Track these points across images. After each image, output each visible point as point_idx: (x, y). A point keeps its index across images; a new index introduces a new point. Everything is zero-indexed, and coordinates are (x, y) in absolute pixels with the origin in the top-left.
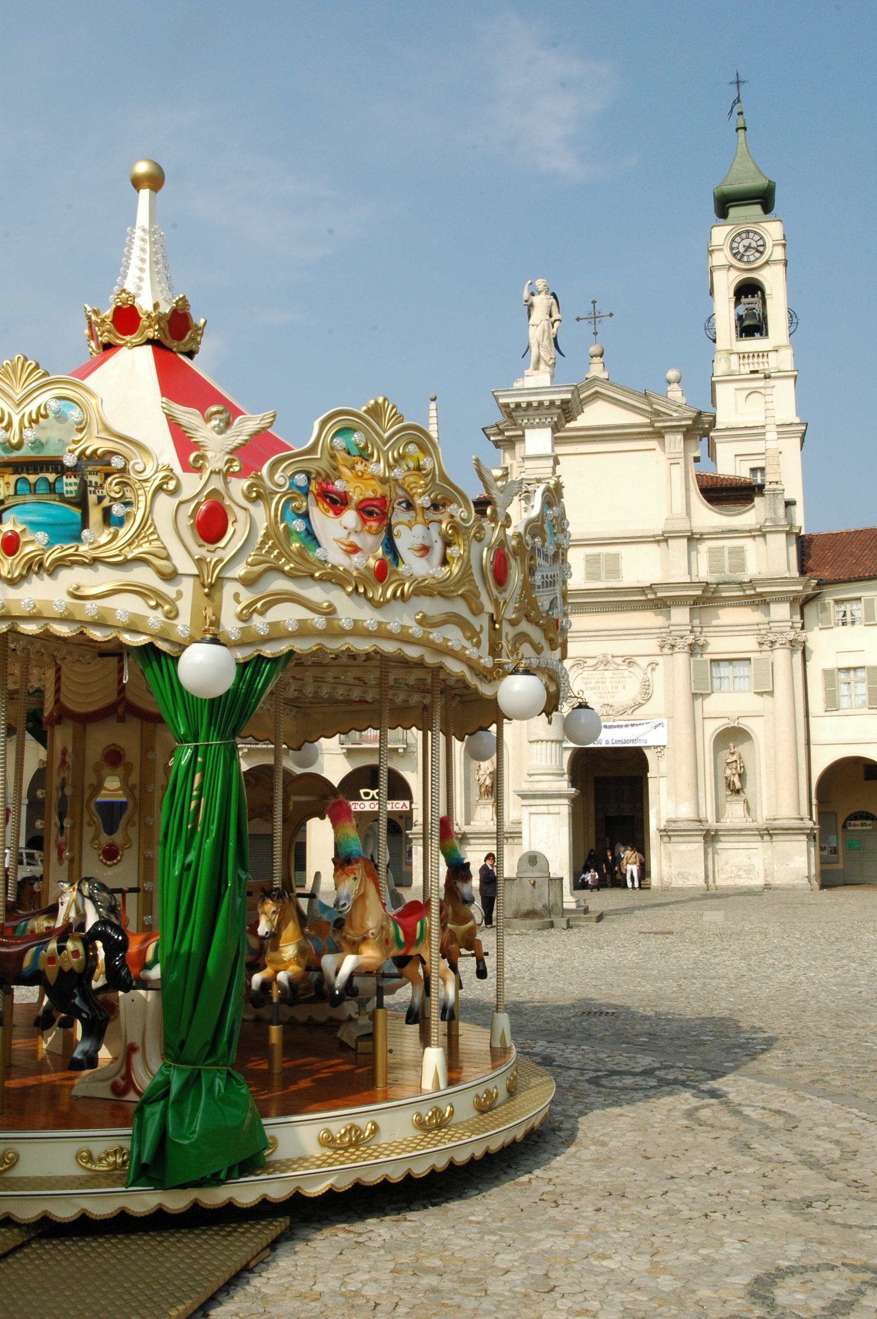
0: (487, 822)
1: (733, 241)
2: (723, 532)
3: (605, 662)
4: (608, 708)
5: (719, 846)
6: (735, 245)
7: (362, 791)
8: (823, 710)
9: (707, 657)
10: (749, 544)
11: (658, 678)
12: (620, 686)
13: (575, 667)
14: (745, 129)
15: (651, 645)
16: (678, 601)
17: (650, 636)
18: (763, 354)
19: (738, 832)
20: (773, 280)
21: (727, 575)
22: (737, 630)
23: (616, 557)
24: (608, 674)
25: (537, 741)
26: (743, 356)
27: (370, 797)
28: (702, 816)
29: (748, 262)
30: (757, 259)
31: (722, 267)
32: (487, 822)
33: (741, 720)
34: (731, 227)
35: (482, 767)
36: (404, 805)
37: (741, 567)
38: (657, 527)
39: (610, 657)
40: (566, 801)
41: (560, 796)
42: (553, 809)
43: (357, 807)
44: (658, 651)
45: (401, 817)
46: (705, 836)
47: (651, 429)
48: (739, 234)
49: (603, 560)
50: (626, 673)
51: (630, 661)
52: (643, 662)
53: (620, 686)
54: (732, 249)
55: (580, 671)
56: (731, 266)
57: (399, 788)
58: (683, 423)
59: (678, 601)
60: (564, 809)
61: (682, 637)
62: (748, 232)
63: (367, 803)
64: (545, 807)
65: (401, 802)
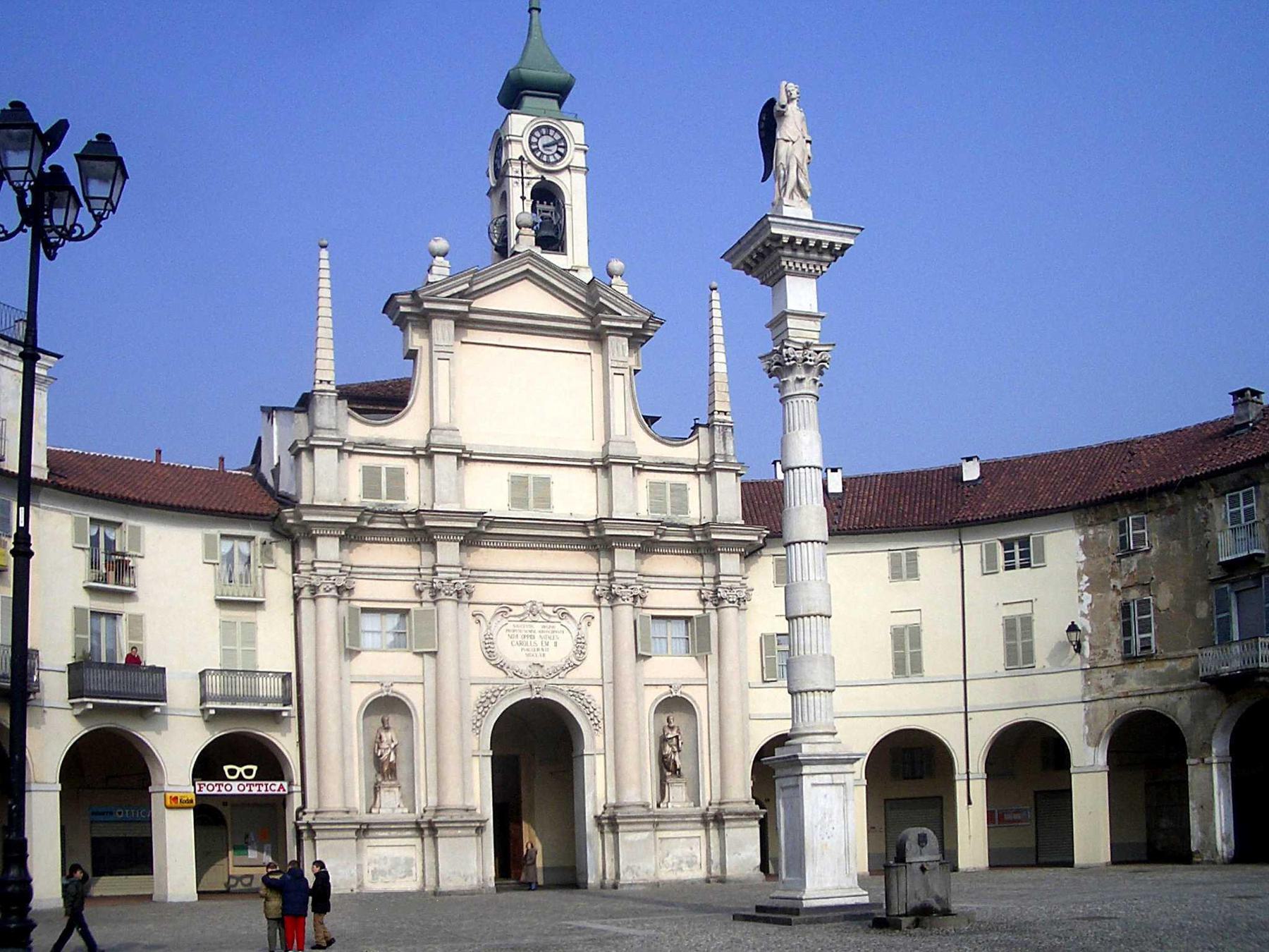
0: (393, 809)
1: (532, 134)
2: (664, 464)
3: (533, 611)
4: (536, 668)
5: (366, 842)
6: (534, 140)
7: (226, 768)
8: (1003, 669)
11: (592, 635)
12: (551, 643)
13: (499, 617)
14: (539, 10)
15: (583, 594)
17: (585, 583)
19: (680, 819)
20: (574, 188)
21: (667, 516)
22: (381, 573)
23: (546, 481)
24: (537, 626)
27: (237, 776)
28: (350, 806)
29: (548, 163)
30: (558, 161)
32: (393, 809)
33: (686, 690)
35: (384, 739)
36: (281, 786)
37: (683, 507)
39: (540, 605)
43: (263, 789)
45: (225, 804)
46: (358, 831)
47: (588, 328)
48: (539, 129)
51: (562, 611)
53: (551, 643)
54: (530, 143)
55: (505, 621)
57: (272, 765)
58: (633, 325)
60: (1104, 777)
62: (548, 128)
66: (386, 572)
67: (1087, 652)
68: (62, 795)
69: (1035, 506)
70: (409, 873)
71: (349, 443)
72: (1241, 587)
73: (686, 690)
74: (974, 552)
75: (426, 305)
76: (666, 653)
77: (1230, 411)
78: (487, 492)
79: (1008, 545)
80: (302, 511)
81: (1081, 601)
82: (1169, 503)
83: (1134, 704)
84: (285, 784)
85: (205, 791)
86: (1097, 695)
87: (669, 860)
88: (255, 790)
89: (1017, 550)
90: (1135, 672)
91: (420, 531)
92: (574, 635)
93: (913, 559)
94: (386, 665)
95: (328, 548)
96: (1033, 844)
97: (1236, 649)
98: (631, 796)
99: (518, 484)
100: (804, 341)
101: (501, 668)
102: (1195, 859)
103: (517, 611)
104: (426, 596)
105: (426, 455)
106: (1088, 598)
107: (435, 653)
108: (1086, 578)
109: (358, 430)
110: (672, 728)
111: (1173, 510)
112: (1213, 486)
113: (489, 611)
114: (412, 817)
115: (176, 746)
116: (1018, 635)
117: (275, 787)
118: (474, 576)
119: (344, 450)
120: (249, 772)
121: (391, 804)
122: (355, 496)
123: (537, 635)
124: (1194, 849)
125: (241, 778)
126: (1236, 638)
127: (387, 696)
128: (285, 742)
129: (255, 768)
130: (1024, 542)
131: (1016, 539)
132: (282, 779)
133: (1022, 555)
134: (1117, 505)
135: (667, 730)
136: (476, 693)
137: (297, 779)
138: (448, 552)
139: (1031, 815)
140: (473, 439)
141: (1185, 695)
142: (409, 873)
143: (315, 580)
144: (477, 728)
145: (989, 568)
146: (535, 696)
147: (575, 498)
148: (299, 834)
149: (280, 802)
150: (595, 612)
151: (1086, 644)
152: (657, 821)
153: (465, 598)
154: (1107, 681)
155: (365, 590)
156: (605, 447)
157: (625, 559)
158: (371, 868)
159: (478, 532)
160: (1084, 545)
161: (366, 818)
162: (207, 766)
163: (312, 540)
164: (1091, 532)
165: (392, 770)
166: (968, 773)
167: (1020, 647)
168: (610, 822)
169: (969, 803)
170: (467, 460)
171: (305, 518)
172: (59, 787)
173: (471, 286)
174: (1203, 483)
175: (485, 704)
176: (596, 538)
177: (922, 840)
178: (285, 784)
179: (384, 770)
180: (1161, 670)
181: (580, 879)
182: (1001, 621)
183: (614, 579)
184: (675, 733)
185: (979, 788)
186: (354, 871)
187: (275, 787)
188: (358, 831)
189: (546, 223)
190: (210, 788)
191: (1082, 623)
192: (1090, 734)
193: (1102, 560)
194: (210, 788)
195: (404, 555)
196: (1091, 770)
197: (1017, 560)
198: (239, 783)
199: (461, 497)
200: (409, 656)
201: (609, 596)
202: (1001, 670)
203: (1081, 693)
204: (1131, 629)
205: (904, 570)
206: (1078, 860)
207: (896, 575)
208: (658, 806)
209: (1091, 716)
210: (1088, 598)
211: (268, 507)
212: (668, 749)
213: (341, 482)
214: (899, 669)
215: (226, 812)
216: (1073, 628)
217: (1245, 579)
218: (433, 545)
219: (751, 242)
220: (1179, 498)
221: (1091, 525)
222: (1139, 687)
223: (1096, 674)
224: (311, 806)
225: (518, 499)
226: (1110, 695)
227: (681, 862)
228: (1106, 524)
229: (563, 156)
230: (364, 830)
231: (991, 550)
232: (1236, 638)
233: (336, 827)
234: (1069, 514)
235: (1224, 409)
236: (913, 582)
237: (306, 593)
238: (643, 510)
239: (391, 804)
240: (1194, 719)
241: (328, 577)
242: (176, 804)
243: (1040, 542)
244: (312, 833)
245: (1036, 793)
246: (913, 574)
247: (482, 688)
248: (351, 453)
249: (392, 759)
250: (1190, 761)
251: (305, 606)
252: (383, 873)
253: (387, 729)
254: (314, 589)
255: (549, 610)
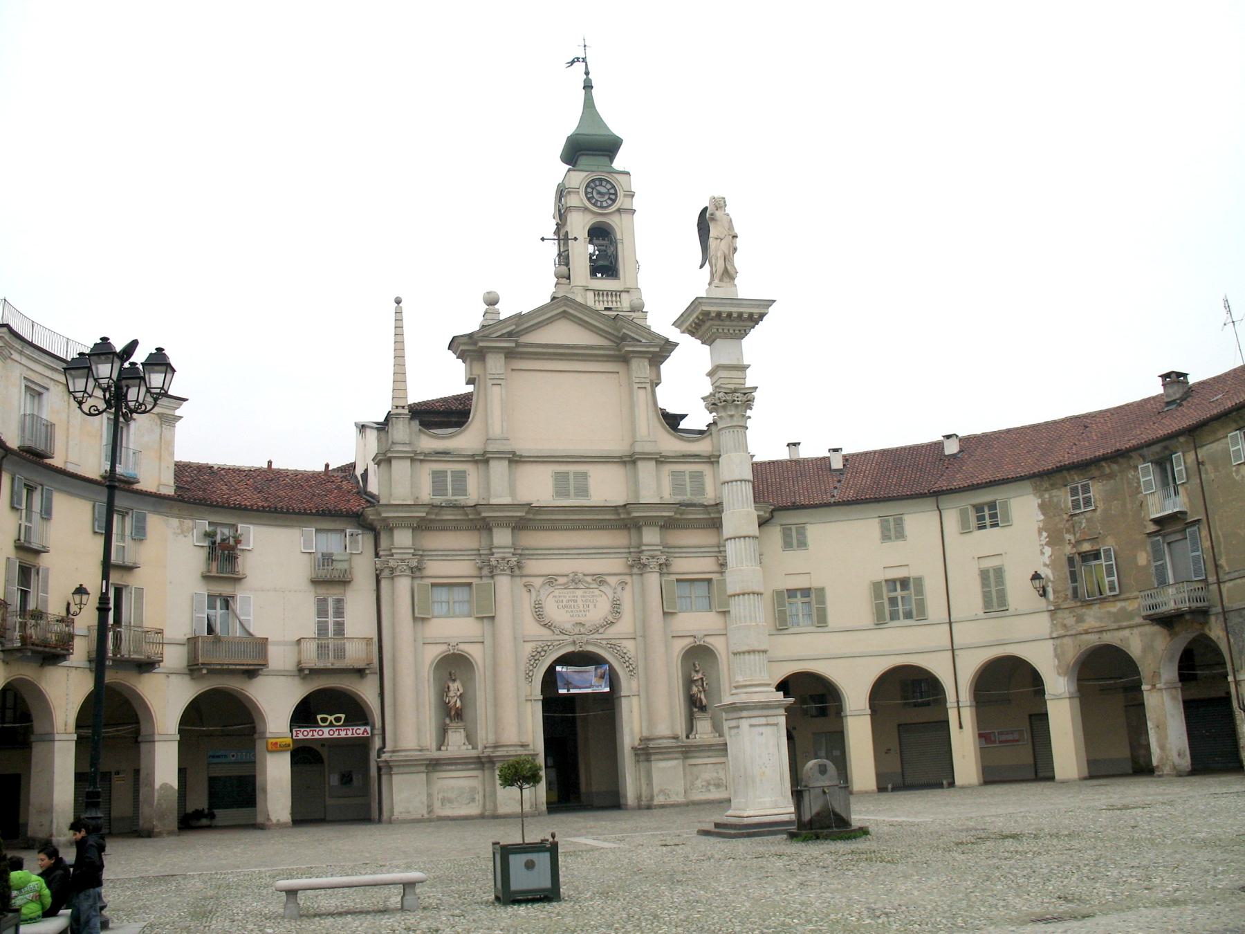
1: (588, 186)
3: (575, 581)
7: (319, 717)
9: (674, 577)
10: (706, 469)
11: (627, 597)
15: (613, 565)
16: (650, 522)
18: (617, 294)
21: (687, 497)
23: (585, 475)
24: (579, 593)
25: (749, 652)
26: (598, 293)
29: (601, 207)
31: (577, 208)
33: (708, 640)
34: (585, 174)
36: (365, 731)
37: (701, 490)
38: (617, 446)
39: (581, 576)
40: (782, 711)
41: (778, 707)
42: (772, 720)
44: (627, 571)
45: (323, 745)
46: (427, 766)
48: (593, 181)
49: (571, 476)
50: (597, 592)
51: (600, 579)
52: (613, 580)
53: (591, 606)
54: (586, 193)
56: (586, 209)
57: (356, 712)
59: (650, 522)
60: (868, 718)
61: (653, 557)
62: (601, 180)
63: (326, 730)
64: (962, 710)
65: (362, 728)
66: (451, 556)
67: (1051, 596)
68: (180, 744)
69: (1000, 476)
70: (473, 800)
71: (421, 453)
72: (1169, 539)
73: (708, 640)
74: (952, 518)
75: (481, 344)
76: (690, 609)
77: (1161, 390)
78: (537, 487)
79: (979, 508)
80: (380, 509)
81: (1042, 553)
82: (1107, 470)
83: (1093, 640)
84: (368, 728)
85: (301, 736)
86: (1062, 632)
87: (699, 783)
88: (343, 734)
89: (987, 513)
90: (1092, 613)
91: (479, 520)
92: (611, 597)
93: (899, 522)
94: (454, 628)
95: (403, 538)
96: (1030, 760)
97: (1171, 591)
98: (663, 729)
99: (561, 478)
100: (732, 387)
101: (549, 628)
102: (404, 795)
103: (562, 580)
104: (485, 572)
105: (482, 459)
106: (1048, 551)
107: (493, 618)
108: (1045, 534)
109: (428, 443)
110: (697, 672)
111: (1111, 476)
112: (1140, 455)
113: (538, 582)
114: (474, 753)
115: (167, 700)
116: (992, 584)
117: (360, 731)
118: (522, 554)
119: (417, 458)
120: (338, 720)
121: (457, 743)
122: (426, 495)
123: (579, 600)
124: (1155, 763)
125: (331, 725)
126: (1171, 582)
127: (454, 654)
128: (367, 692)
129: (343, 716)
130: (992, 506)
131: (986, 504)
132: (366, 724)
133: (989, 517)
134: (1065, 473)
135: (693, 674)
136: (529, 648)
137: (378, 724)
138: (502, 537)
139: (1027, 736)
140: (524, 445)
141: (1136, 631)
142: (473, 800)
143: (392, 563)
144: (529, 678)
145: (965, 529)
146: (577, 649)
147: (606, 488)
148: (379, 769)
149: (362, 745)
150: (628, 579)
151: (1050, 589)
152: (687, 752)
153: (517, 572)
154: (1070, 621)
155: (436, 568)
156: (632, 445)
157: (651, 537)
158: (440, 796)
159: (528, 519)
160: (1042, 507)
161: (437, 755)
162: (304, 714)
163: (390, 530)
164: (1047, 496)
165: (458, 715)
166: (958, 702)
167: (994, 594)
168: (645, 752)
169: (961, 727)
170: (517, 462)
171: (384, 515)
172: (178, 737)
173: (517, 325)
174: (1132, 454)
175: (535, 658)
176: (625, 519)
177: (823, 770)
178: (368, 728)
179: (453, 714)
180: (1114, 610)
181: (622, 801)
182: (977, 572)
183: (641, 552)
184: (700, 675)
185: (968, 715)
186: (424, 799)
187: (360, 731)
188: (427, 766)
189: (603, 254)
190: (305, 734)
191: (1046, 572)
192: (1059, 666)
193: (1057, 519)
194: (305, 734)
195: (466, 541)
196: (1057, 698)
197: (988, 521)
198: (327, 730)
199: (512, 491)
200: (471, 620)
201: (638, 565)
202: (981, 614)
203: (1048, 631)
204: (1079, 576)
205: (893, 532)
206: (1057, 777)
207: (886, 537)
208: (688, 737)
209: (1059, 651)
210: (1048, 551)
211: (355, 505)
212: (695, 689)
213: (414, 484)
214: (880, 621)
215: (324, 753)
216: (1036, 576)
217: (1175, 532)
218: (490, 530)
219: (690, 315)
220: (1115, 467)
221: (1046, 490)
222: (1097, 624)
223: (1060, 614)
224: (389, 747)
225: (561, 492)
226: (1073, 632)
227: (709, 784)
228: (1059, 489)
229: (614, 201)
230: (434, 765)
231: (963, 513)
232: (1171, 582)
233: (410, 765)
234: (1027, 483)
235: (1156, 389)
236: (900, 543)
237: (386, 573)
238: (668, 496)
239: (457, 743)
240: (1144, 651)
241: (403, 561)
242: (277, 748)
243: (1005, 505)
244: (390, 768)
245: (1030, 716)
246: (900, 535)
247: (533, 645)
248: (421, 461)
249: (458, 704)
250: (1144, 687)
251: (384, 583)
252: (450, 801)
253: (454, 681)
254: (392, 570)
255: (589, 579)
